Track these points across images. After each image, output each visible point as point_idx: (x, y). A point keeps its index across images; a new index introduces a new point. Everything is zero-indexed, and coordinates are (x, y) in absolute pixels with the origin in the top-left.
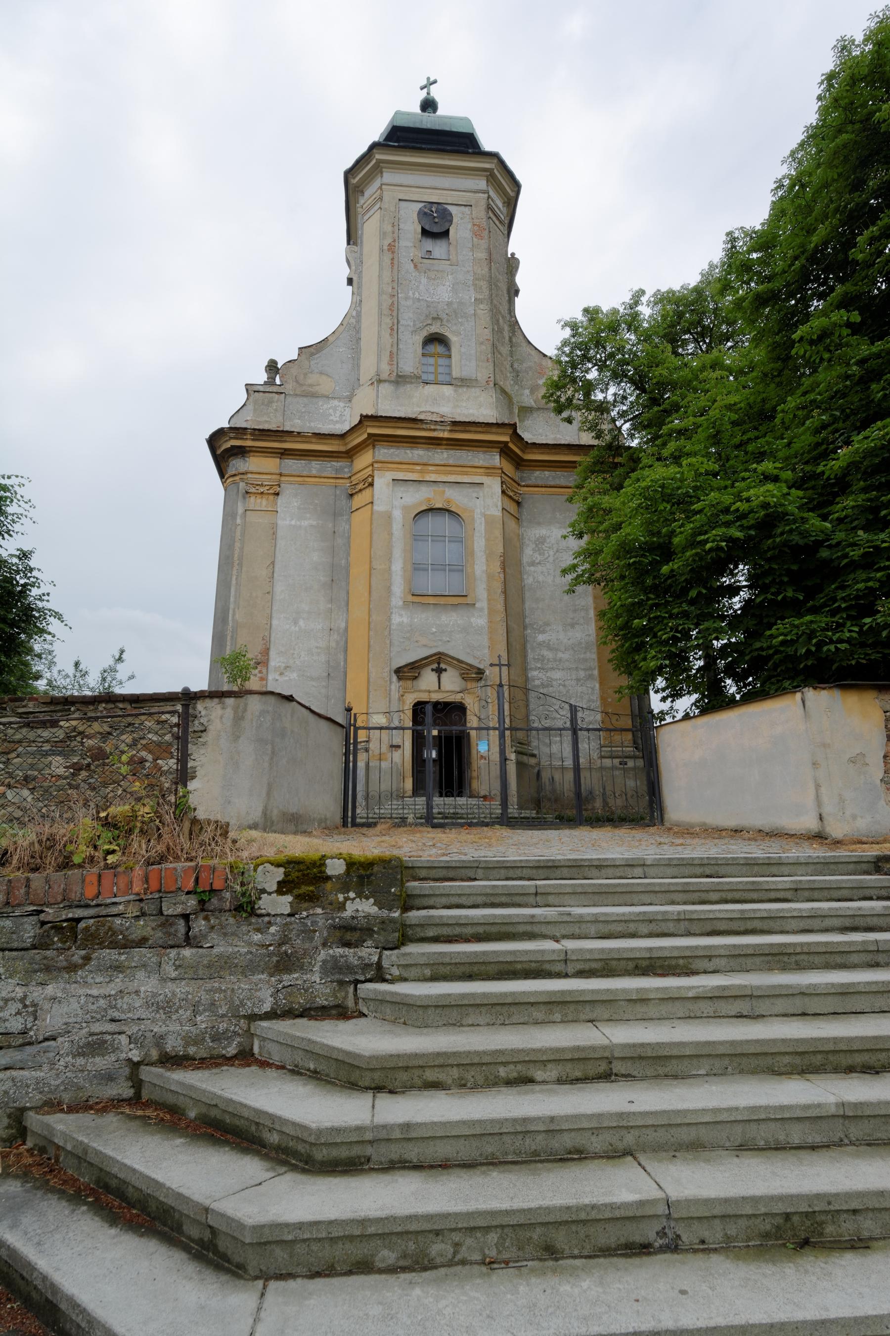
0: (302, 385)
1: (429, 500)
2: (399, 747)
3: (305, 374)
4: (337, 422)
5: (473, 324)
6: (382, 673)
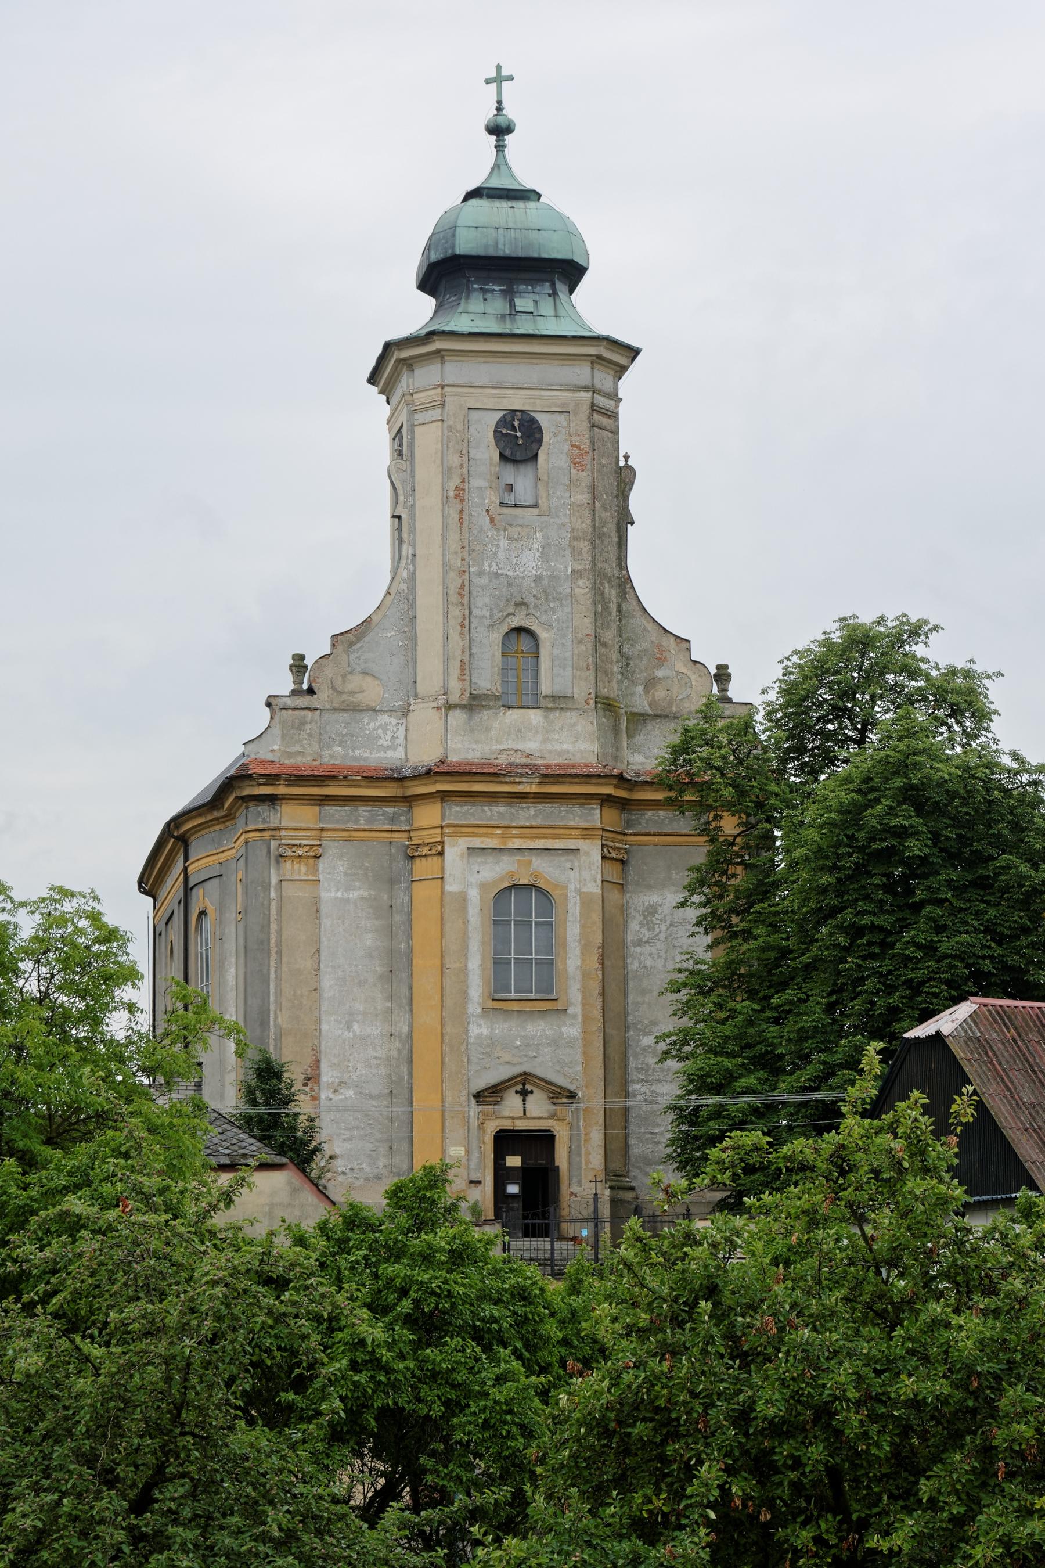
0: (339, 693)
1: (512, 874)
2: (479, 1182)
3: (344, 676)
4: (388, 748)
5: (569, 610)
6: (459, 1097)
